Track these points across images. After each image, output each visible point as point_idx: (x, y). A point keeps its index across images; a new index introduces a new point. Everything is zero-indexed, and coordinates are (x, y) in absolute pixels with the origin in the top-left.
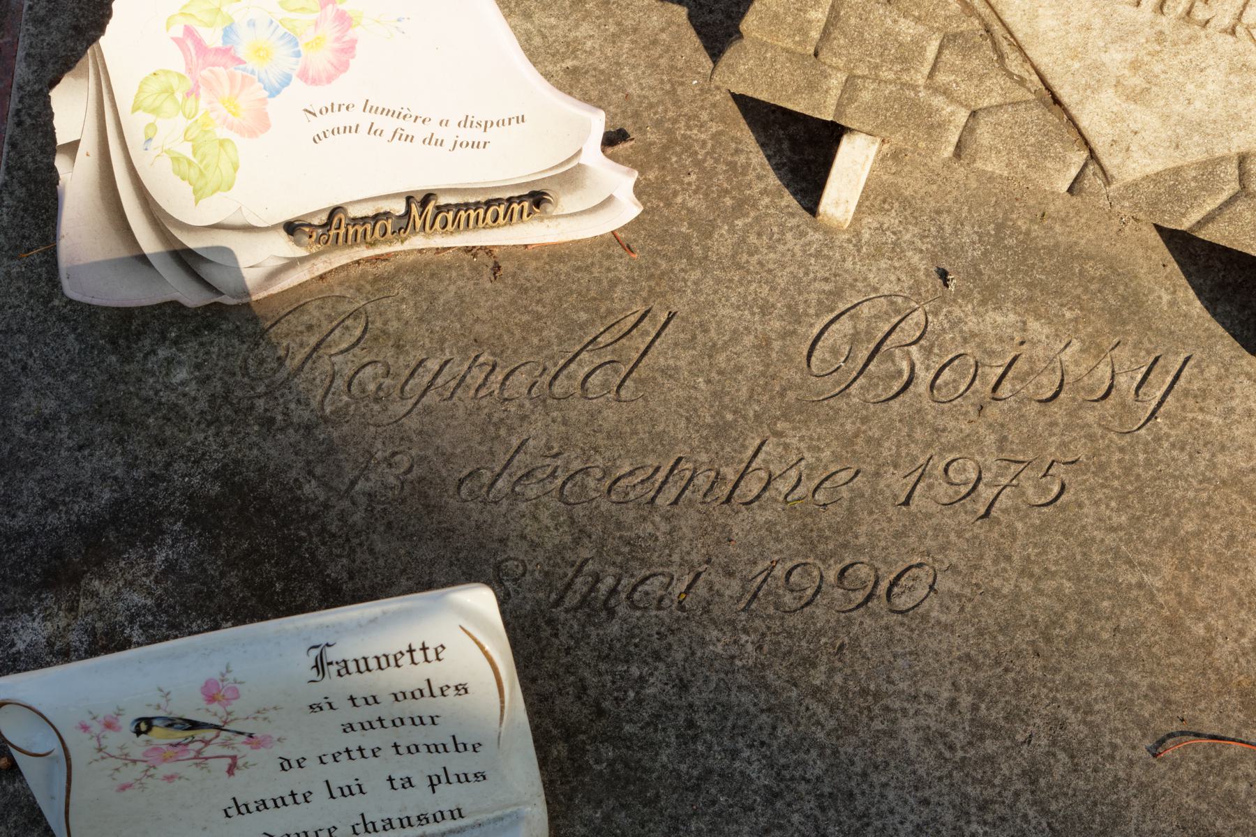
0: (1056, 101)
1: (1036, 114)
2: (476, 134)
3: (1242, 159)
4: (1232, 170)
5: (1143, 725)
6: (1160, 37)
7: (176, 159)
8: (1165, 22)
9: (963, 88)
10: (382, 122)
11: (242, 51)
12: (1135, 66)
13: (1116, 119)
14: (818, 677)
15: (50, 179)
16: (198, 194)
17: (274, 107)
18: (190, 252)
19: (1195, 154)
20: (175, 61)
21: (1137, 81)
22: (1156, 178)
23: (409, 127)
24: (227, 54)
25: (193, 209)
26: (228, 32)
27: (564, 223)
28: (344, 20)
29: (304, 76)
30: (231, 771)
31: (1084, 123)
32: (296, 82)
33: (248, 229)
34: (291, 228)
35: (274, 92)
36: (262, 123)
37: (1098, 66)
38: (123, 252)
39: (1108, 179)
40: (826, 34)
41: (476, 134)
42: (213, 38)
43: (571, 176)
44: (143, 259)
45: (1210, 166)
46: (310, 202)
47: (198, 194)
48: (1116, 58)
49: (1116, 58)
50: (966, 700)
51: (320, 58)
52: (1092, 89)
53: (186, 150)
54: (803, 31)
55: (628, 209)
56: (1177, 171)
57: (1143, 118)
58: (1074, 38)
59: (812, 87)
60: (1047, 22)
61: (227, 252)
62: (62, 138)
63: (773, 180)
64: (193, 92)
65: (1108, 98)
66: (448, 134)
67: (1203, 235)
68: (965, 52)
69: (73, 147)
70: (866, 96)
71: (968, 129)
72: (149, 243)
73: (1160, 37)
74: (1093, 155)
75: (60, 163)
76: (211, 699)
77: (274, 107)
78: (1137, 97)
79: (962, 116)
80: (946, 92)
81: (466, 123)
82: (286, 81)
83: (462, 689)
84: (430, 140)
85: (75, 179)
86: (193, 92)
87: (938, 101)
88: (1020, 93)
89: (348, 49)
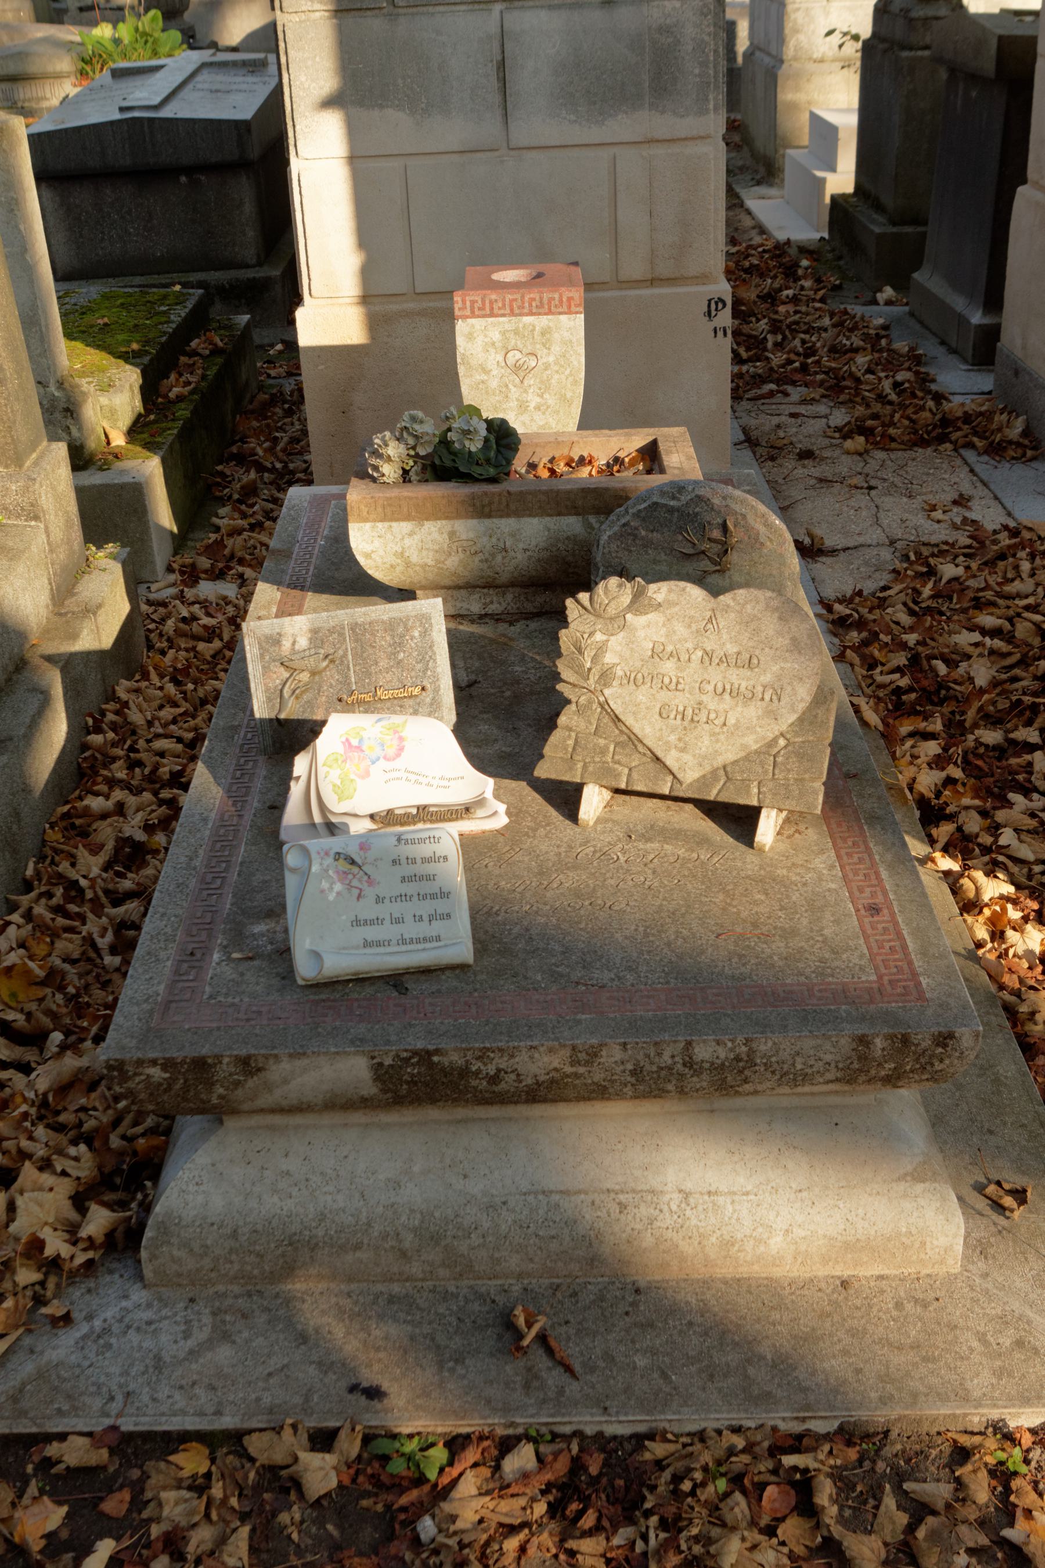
0: (658, 759)
1: (651, 765)
2: (445, 783)
3: (724, 767)
4: (722, 772)
5: (713, 932)
6: (685, 729)
7: (334, 785)
8: (686, 723)
9: (624, 760)
10: (413, 777)
11: (364, 748)
12: (680, 740)
13: (678, 760)
14: (582, 926)
15: (288, 788)
16: (340, 800)
17: (373, 769)
18: (332, 824)
19: (708, 768)
20: (340, 749)
21: (681, 745)
22: (698, 780)
23: (421, 779)
24: (359, 748)
25: (336, 806)
26: (361, 740)
27: (478, 822)
28: (401, 739)
29: (385, 758)
30: (359, 897)
31: (668, 763)
32: (382, 760)
33: (356, 816)
34: (372, 817)
35: (373, 763)
36: (367, 774)
37: (667, 743)
38: (306, 821)
39: (681, 783)
40: (574, 749)
41: (445, 783)
42: (355, 742)
43: (480, 802)
44: (314, 825)
45: (714, 772)
46: (380, 806)
47: (340, 800)
48: (673, 738)
49: (673, 738)
50: (641, 929)
51: (391, 752)
52: (668, 750)
53: (338, 782)
54: (566, 749)
55: (502, 820)
56: (704, 776)
57: (687, 757)
58: (658, 734)
59: (571, 769)
60: (648, 730)
61: (346, 825)
62: (295, 774)
63: (561, 818)
64: (344, 761)
65: (674, 753)
66: (435, 783)
67: (719, 799)
68: (623, 748)
69: (298, 778)
70: (591, 769)
71: (629, 775)
72: (317, 818)
73: (685, 729)
74: (675, 777)
75: (292, 784)
76: (361, 849)
77: (373, 769)
78: (683, 750)
79: (626, 771)
80: (619, 763)
81: (442, 778)
82: (378, 759)
83: (445, 858)
84: (428, 785)
85: (296, 790)
86: (344, 761)
87: (616, 766)
88: (644, 759)
89: (401, 749)
